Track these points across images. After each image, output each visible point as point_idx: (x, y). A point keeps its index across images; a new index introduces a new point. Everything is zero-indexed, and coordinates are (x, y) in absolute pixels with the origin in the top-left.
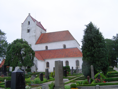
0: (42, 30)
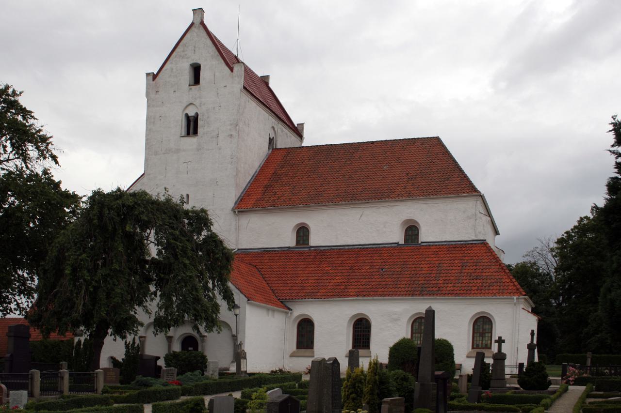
0: (280, 127)
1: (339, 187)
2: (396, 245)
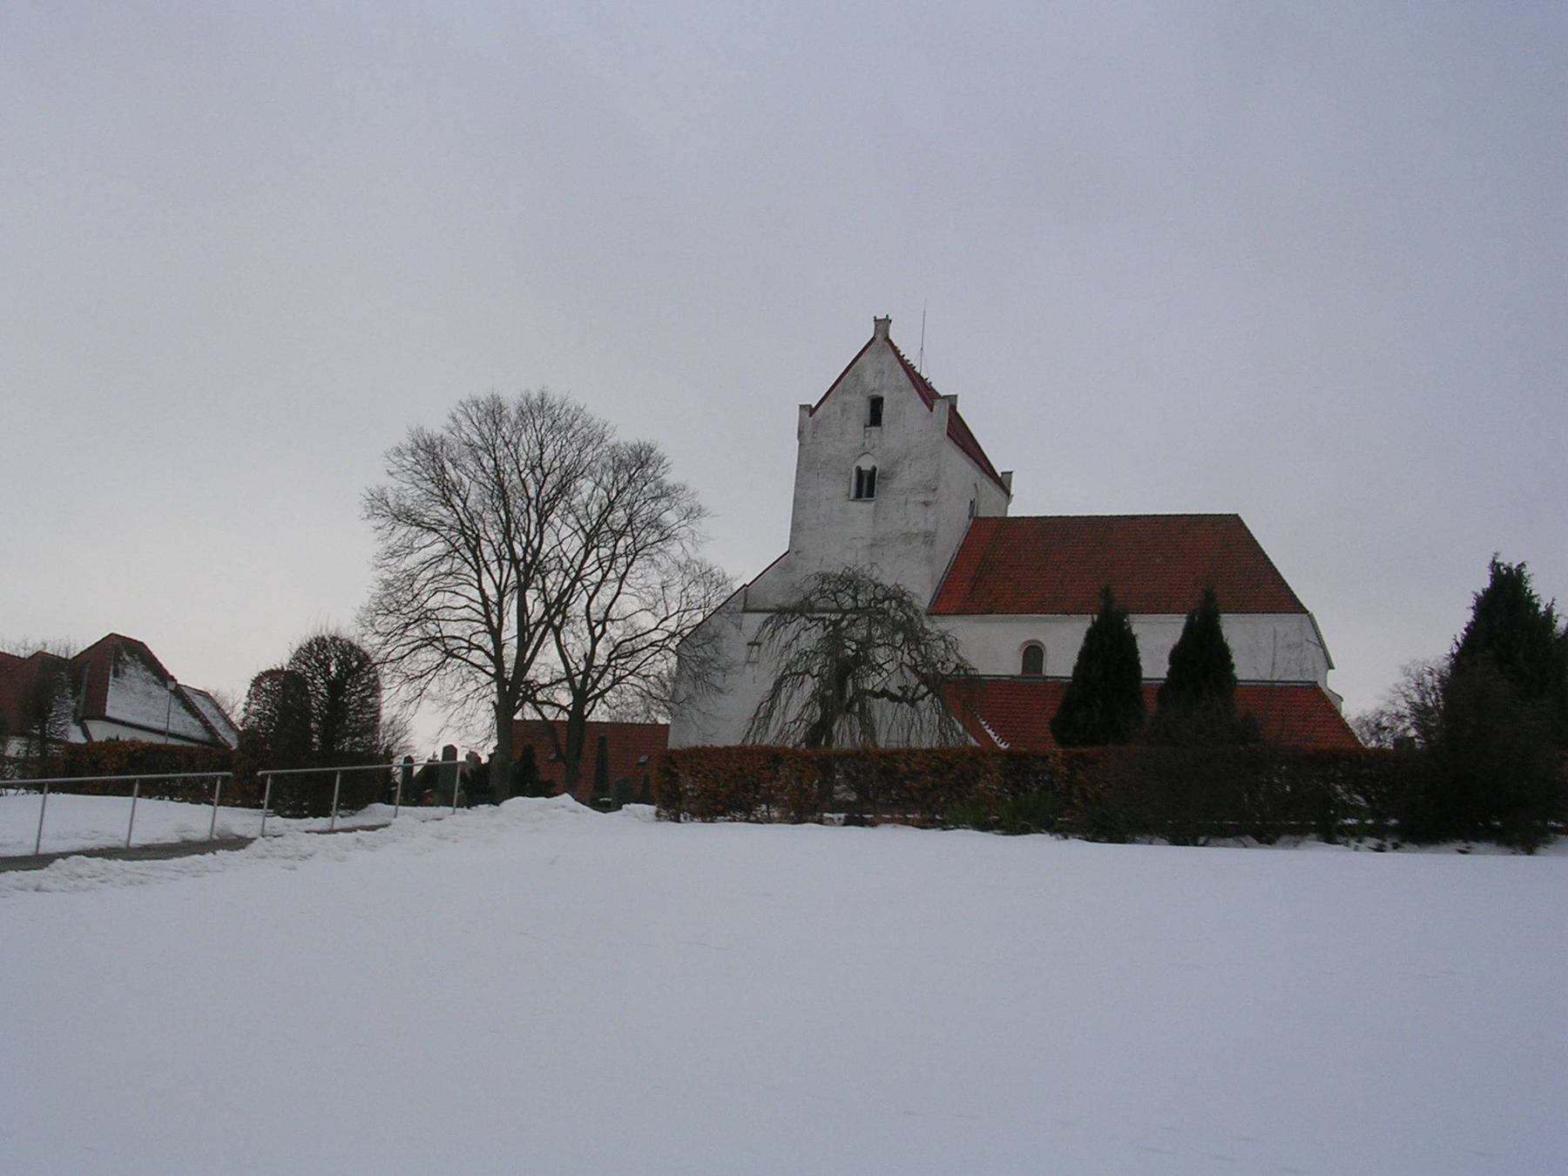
1: (1073, 576)
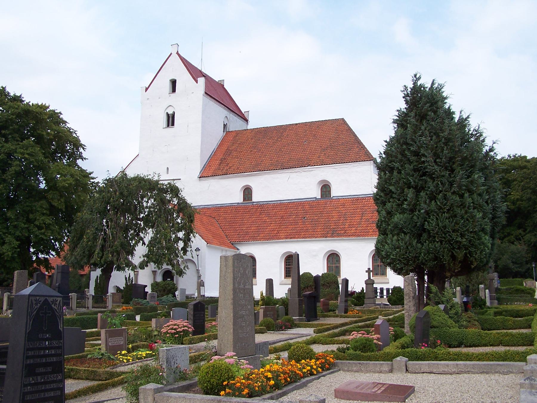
0: (231, 116)
2: (315, 199)
